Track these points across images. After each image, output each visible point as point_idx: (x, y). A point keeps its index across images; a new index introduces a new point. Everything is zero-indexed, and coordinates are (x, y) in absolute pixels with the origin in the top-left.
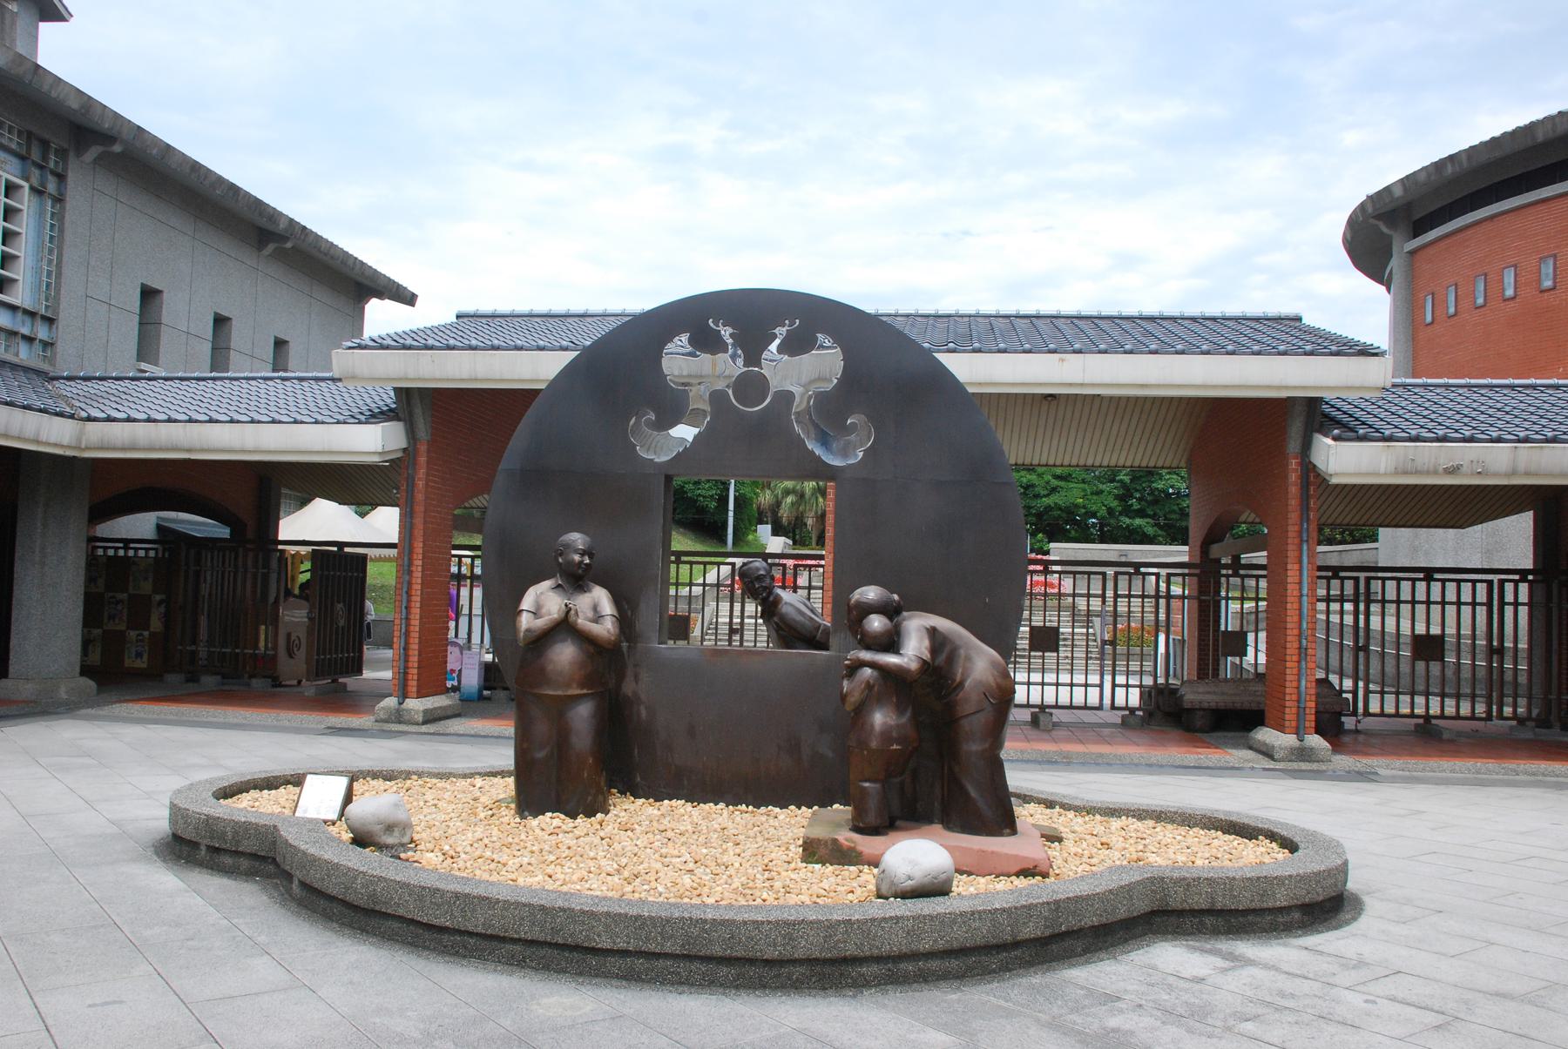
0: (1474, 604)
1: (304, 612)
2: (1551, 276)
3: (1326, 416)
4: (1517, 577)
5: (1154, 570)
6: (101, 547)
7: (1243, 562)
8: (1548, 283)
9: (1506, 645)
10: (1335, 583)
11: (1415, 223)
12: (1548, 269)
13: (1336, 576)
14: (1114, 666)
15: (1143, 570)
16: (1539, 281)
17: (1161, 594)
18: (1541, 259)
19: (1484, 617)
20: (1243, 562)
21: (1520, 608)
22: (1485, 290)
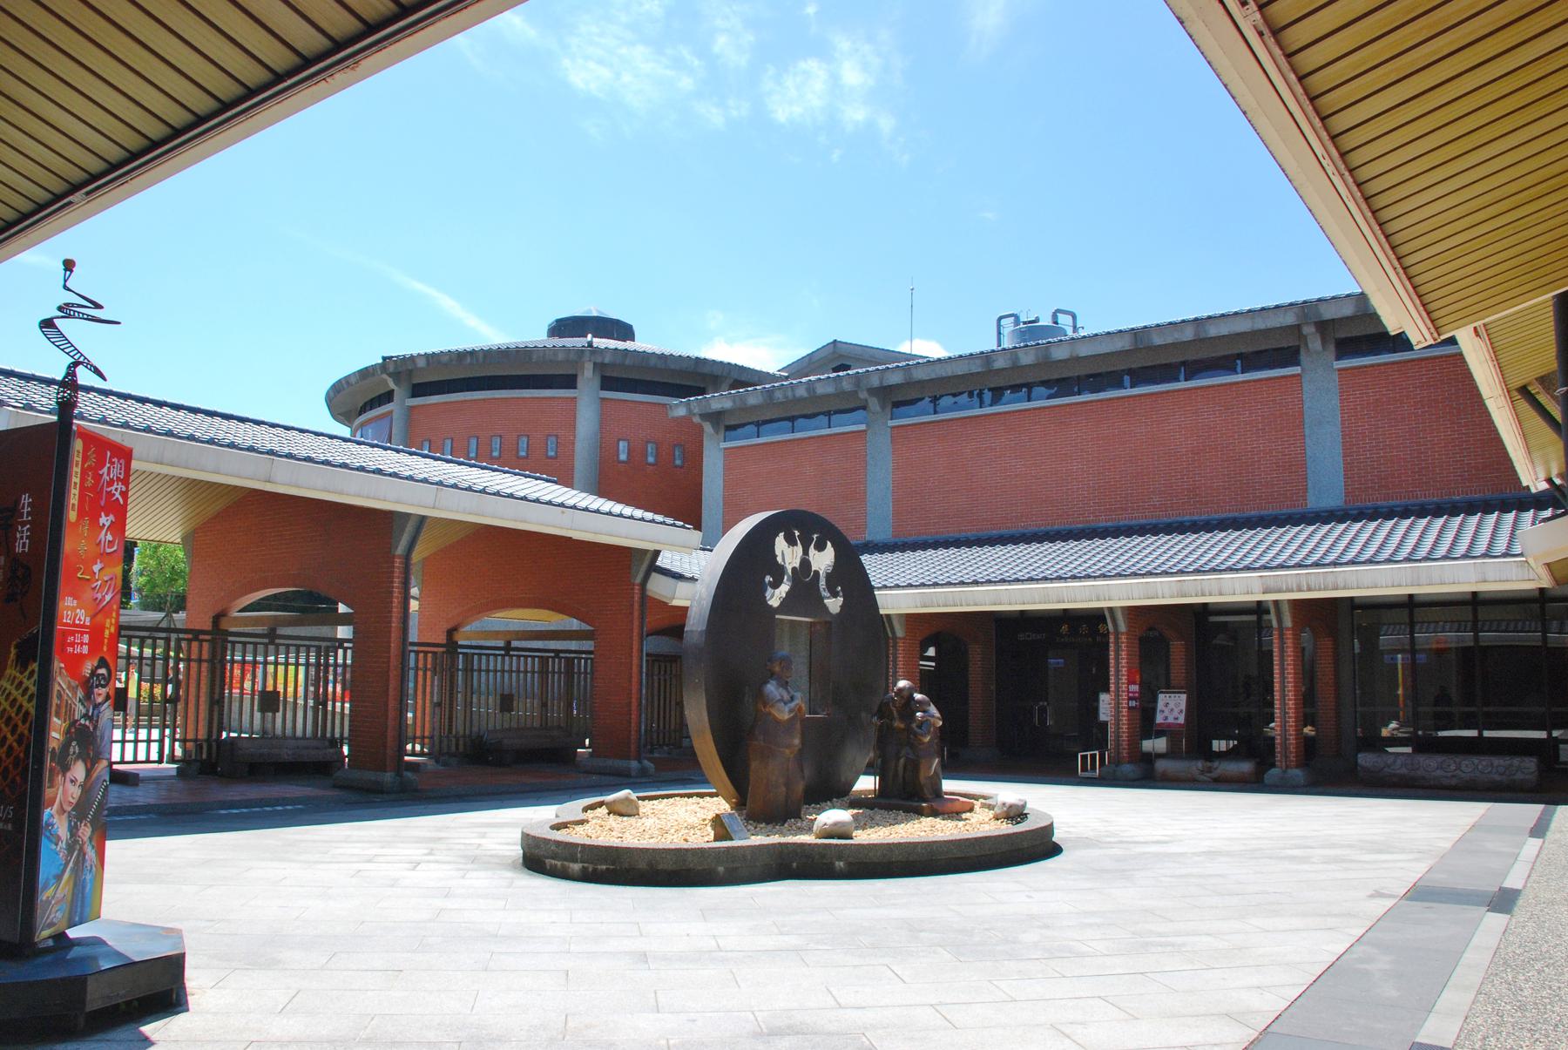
0: (200, 661)
1: (769, 686)
2: (525, 449)
3: (1182, 688)
4: (190, 636)
5: (317, 643)
6: (284, 645)
7: (512, 646)
8: (523, 454)
9: (288, 699)
10: (195, 644)
11: (414, 386)
12: (523, 442)
13: (196, 638)
14: (138, 720)
15: (201, 637)
16: (518, 451)
17: (157, 656)
18: (518, 436)
19: (283, 672)
20: (512, 646)
21: (290, 667)
22: (477, 448)
